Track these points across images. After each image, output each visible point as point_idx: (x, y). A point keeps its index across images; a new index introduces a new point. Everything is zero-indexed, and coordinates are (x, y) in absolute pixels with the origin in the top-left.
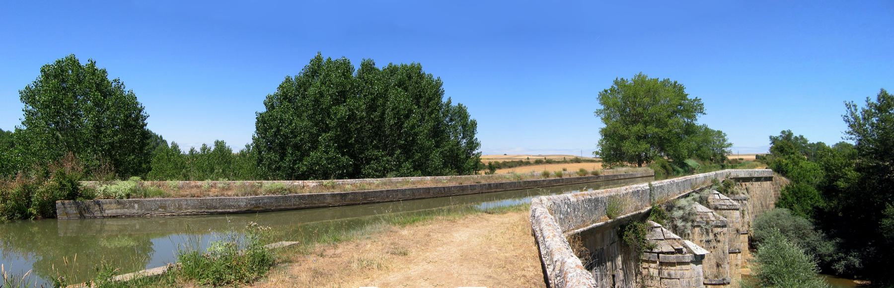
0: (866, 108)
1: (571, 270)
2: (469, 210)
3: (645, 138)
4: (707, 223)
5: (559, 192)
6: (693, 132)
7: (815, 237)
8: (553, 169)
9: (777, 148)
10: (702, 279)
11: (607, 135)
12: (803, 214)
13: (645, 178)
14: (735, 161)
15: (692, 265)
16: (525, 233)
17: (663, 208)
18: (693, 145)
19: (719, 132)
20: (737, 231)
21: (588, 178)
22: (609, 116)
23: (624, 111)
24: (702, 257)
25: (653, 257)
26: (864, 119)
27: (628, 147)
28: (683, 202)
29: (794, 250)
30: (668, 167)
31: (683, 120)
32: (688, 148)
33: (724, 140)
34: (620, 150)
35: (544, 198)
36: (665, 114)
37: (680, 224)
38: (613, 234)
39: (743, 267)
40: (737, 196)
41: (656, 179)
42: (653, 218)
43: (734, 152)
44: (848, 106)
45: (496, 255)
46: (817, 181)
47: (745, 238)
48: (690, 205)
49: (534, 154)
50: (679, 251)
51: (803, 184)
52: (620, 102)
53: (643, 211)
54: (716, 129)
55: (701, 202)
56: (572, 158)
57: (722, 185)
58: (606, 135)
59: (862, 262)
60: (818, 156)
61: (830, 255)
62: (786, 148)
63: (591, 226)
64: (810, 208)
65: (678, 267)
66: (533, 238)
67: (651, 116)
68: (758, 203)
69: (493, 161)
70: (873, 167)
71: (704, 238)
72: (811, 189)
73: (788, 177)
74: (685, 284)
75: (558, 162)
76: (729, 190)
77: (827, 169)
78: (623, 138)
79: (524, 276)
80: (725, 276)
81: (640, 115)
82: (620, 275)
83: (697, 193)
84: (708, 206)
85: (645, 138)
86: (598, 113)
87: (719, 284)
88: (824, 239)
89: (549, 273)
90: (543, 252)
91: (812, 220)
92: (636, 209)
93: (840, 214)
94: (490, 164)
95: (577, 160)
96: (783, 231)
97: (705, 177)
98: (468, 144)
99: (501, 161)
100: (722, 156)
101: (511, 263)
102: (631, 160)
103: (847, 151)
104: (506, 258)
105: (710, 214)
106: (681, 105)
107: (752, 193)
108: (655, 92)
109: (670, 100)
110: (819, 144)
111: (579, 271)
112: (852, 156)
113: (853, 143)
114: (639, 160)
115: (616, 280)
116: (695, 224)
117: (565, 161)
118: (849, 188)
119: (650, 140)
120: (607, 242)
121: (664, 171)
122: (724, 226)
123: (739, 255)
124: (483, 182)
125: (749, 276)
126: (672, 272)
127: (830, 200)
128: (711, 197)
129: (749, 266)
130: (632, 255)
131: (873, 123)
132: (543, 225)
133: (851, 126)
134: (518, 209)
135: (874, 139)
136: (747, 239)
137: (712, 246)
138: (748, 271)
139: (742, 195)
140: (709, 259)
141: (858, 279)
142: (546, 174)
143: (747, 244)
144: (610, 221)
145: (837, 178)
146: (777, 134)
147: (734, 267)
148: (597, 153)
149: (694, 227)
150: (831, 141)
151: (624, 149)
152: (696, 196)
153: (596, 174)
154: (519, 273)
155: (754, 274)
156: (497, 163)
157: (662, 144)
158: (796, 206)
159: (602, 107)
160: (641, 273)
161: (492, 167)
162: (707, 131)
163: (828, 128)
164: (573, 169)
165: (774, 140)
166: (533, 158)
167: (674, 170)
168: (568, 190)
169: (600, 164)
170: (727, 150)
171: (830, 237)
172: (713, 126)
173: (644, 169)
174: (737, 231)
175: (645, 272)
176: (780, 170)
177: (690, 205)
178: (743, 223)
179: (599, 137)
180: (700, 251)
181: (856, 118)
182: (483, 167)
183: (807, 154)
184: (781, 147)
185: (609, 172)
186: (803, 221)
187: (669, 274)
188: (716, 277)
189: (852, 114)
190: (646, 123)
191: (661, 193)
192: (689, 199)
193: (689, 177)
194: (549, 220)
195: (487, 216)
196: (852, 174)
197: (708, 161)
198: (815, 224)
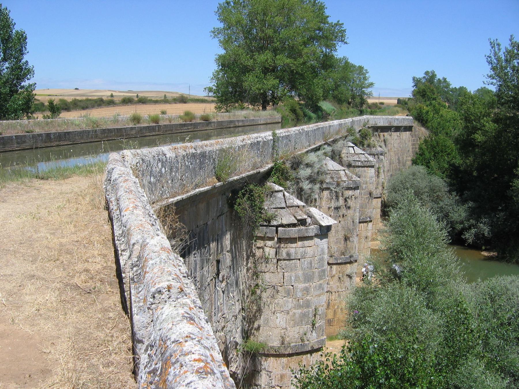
0: (510, 48)
1: (153, 255)
2: (18, 174)
3: (273, 70)
4: (338, 185)
5: (152, 144)
6: (331, 66)
7: (448, 201)
8: (146, 112)
9: (419, 92)
10: (326, 257)
11: (226, 65)
12: (439, 172)
13: (269, 125)
14: (375, 105)
15: (316, 240)
16: (94, 206)
17: (288, 165)
18: (330, 83)
19: (361, 68)
20: (370, 194)
21: (195, 125)
22: (230, 38)
23: (249, 32)
24: (329, 228)
25: (270, 232)
26: (506, 61)
27: (251, 83)
28: (312, 157)
29: (427, 216)
30: (299, 111)
31: (320, 49)
32: (323, 87)
33: (365, 79)
34: (241, 87)
35: (127, 152)
36: (300, 39)
37: (306, 186)
38: (221, 203)
39: (373, 240)
40: (373, 150)
41: (283, 127)
42: (274, 178)
43: (375, 94)
44: (492, 45)
45: (45, 242)
46: (456, 133)
47: (377, 203)
48: (320, 161)
49: (120, 90)
50: (302, 222)
51: (442, 136)
52: (245, 21)
53: (262, 170)
54: (357, 65)
55: (333, 158)
56: (175, 96)
57: (358, 136)
58: (223, 65)
59: (491, 230)
60: (459, 103)
61: (462, 222)
62: (429, 91)
63: (192, 193)
64: (447, 166)
65: (300, 243)
66: (106, 213)
67: (283, 41)
68: (394, 159)
69: (56, 101)
70: (510, 118)
71: (333, 205)
72: (450, 143)
73: (427, 128)
74: (306, 265)
75: (156, 102)
76: (366, 142)
77: (467, 119)
78: (246, 70)
79: (87, 271)
80: (352, 252)
81: (269, 39)
82: (227, 259)
83: (329, 145)
84: (341, 163)
85: (273, 70)
86: (216, 32)
87: (345, 263)
88: (457, 203)
89: (122, 263)
90: (118, 232)
91: (448, 180)
92: (255, 167)
93: (475, 174)
94: (51, 103)
95: (183, 100)
96: (418, 194)
97: (340, 125)
98: (12, 69)
99: (69, 99)
100: (362, 99)
101: (68, 252)
102: (254, 101)
103: (487, 99)
104: (61, 245)
105: (342, 173)
106: (320, 29)
107: (389, 146)
108: (290, 10)
109: (308, 22)
110: (461, 88)
111: (164, 255)
112: (491, 105)
113: (493, 89)
114: (263, 100)
115: (222, 266)
116: (325, 186)
117: (165, 101)
118: (485, 142)
119: (279, 74)
120: (213, 213)
121: (293, 116)
122: (356, 188)
123: (370, 224)
124: (38, 131)
125: (379, 251)
126: (292, 251)
127: (467, 157)
128: (344, 151)
129: (379, 238)
130: (245, 231)
131: (514, 66)
132: (121, 192)
133: (493, 69)
134: (88, 171)
135: (514, 86)
136: (380, 205)
137: (341, 214)
138: (377, 244)
139: (379, 149)
140: (337, 231)
141: (486, 250)
142: (136, 119)
143: (379, 211)
144: (218, 184)
145: (475, 130)
146: (420, 75)
147: (363, 240)
148: (210, 90)
149: (322, 190)
150: (472, 88)
151: (246, 85)
152: (328, 149)
153: (206, 119)
154: (80, 267)
155: (383, 247)
156: (63, 102)
157: (293, 79)
158: (432, 163)
159: (221, 25)
160: (254, 255)
161: (54, 109)
162: (347, 66)
163: (471, 75)
164: (175, 111)
165: (417, 82)
166: (119, 95)
167: (305, 115)
168: (165, 143)
169: (213, 105)
170: (367, 91)
171: (463, 201)
172: (355, 61)
173: (269, 113)
174: (370, 194)
175: (258, 253)
176: (421, 119)
177: (320, 161)
178: (377, 184)
179: (214, 67)
180: (326, 221)
181: (499, 60)
182: (40, 108)
183: (448, 101)
184: (424, 91)
185: (224, 116)
186: (439, 182)
187: (288, 254)
188: (343, 254)
189: (495, 54)
190: (275, 51)
191: (287, 145)
192: (319, 153)
193: (321, 124)
194: (130, 184)
195: (37, 183)
196: (490, 126)
197: (345, 104)
198: (450, 185)
